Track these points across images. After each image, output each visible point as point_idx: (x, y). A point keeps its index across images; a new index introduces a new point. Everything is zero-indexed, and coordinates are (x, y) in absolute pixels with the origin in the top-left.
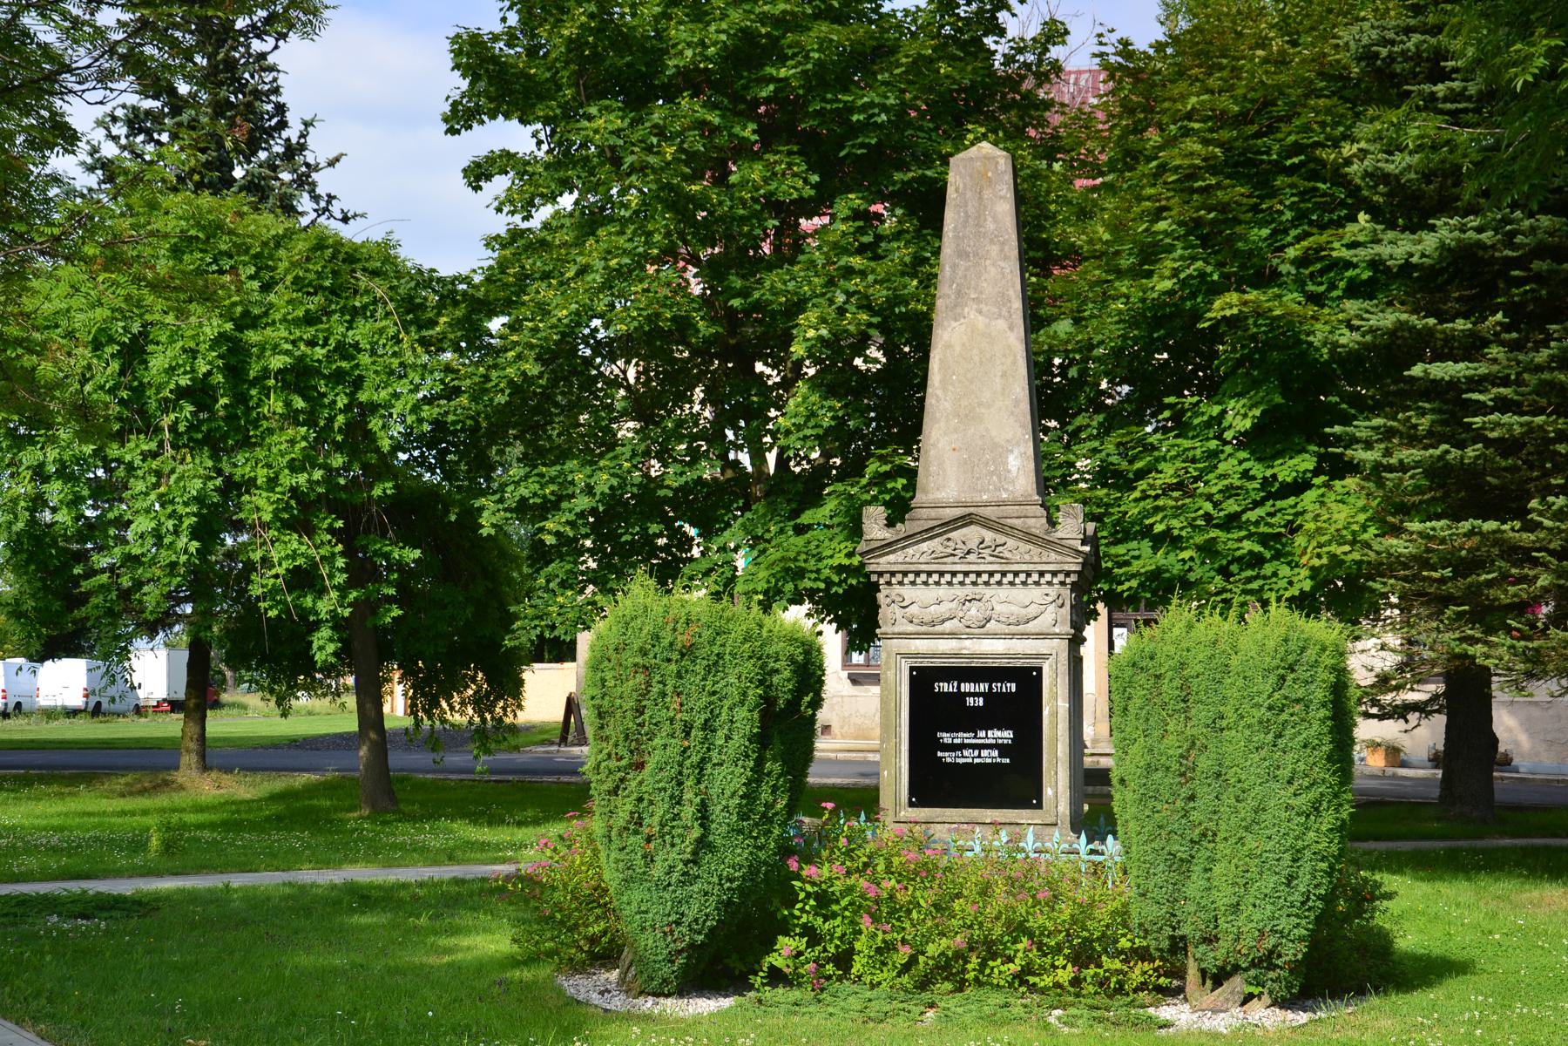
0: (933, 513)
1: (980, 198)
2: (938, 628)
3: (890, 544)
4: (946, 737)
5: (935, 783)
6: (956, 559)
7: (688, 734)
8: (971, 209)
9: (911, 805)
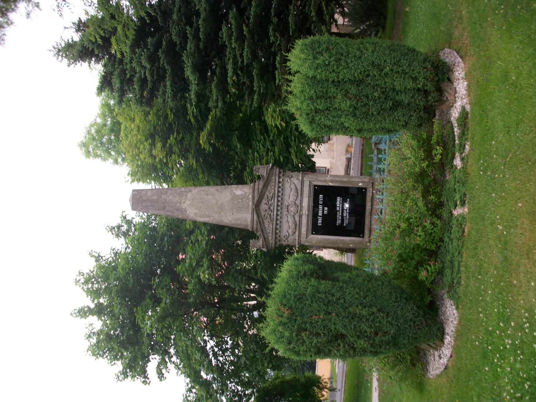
0: (255, 223)
1: (145, 200)
2: (298, 223)
3: (265, 238)
4: (339, 222)
5: (357, 228)
6: (272, 214)
7: (330, 313)
8: (149, 204)
9: (363, 237)
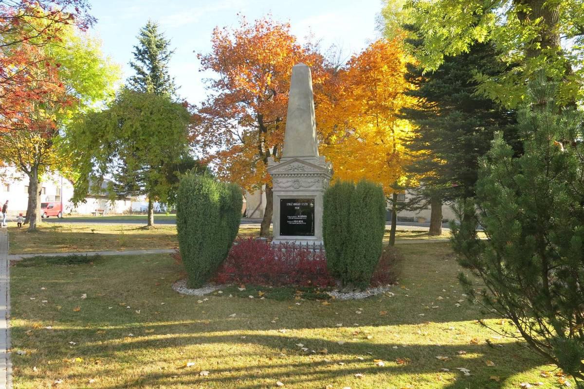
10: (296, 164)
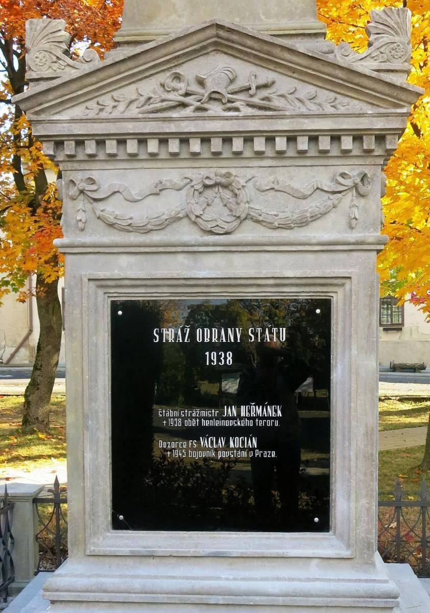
5: (150, 495)
6: (188, 112)
10: (216, 68)
